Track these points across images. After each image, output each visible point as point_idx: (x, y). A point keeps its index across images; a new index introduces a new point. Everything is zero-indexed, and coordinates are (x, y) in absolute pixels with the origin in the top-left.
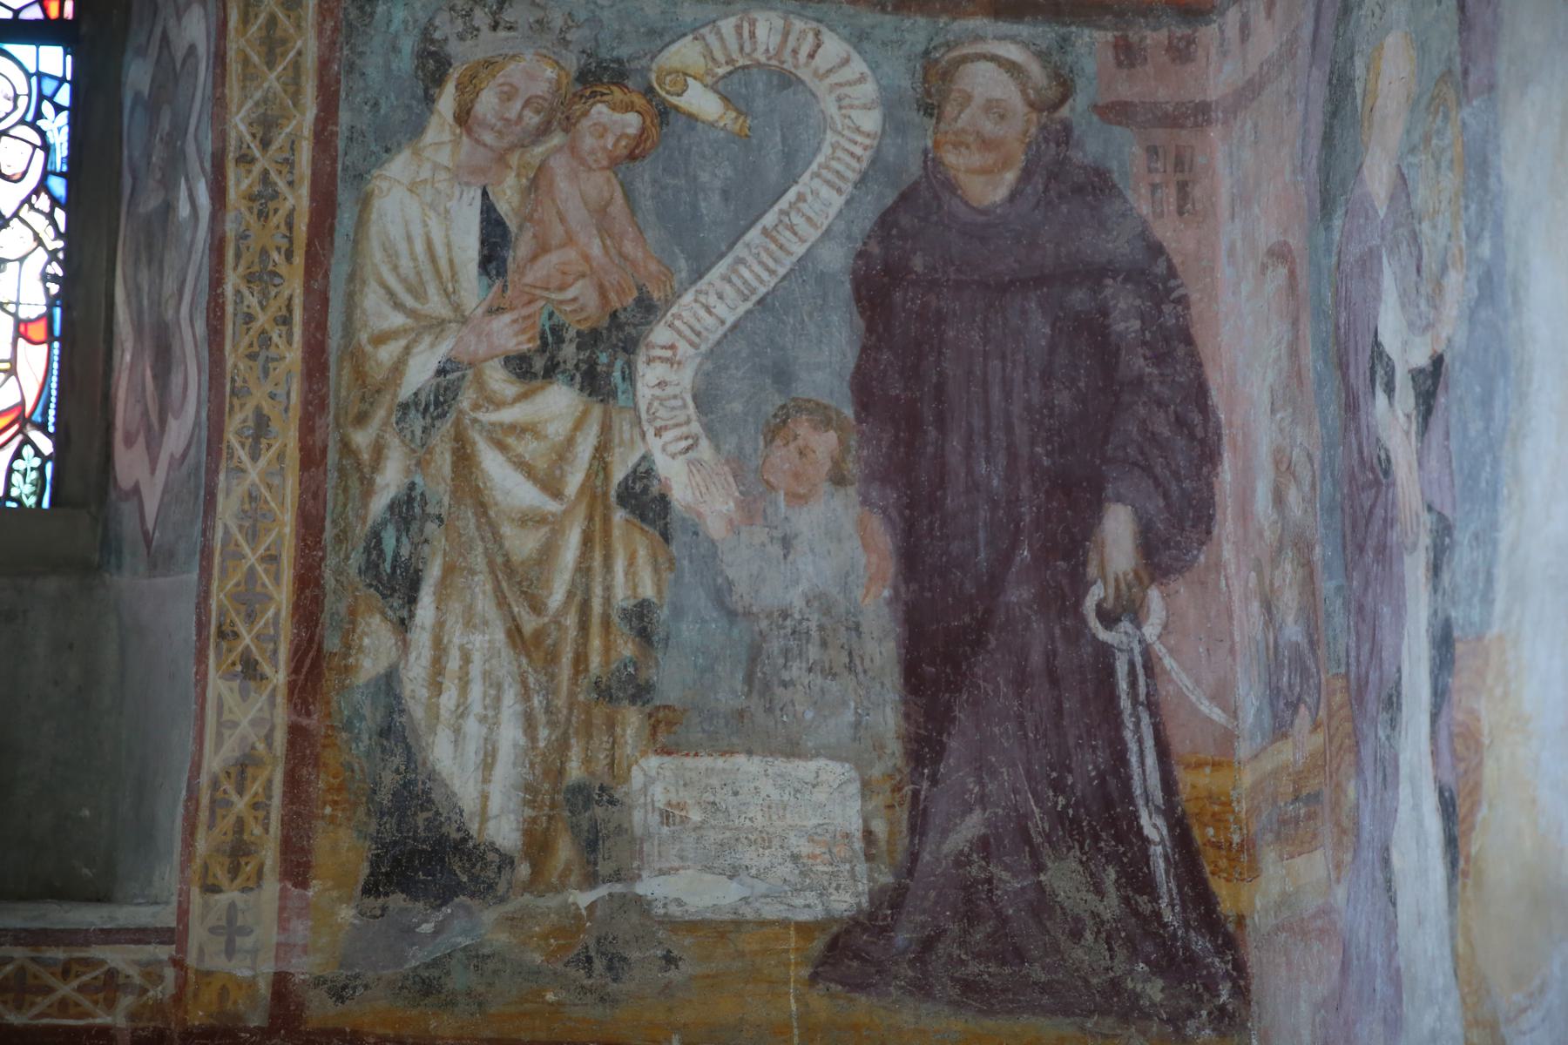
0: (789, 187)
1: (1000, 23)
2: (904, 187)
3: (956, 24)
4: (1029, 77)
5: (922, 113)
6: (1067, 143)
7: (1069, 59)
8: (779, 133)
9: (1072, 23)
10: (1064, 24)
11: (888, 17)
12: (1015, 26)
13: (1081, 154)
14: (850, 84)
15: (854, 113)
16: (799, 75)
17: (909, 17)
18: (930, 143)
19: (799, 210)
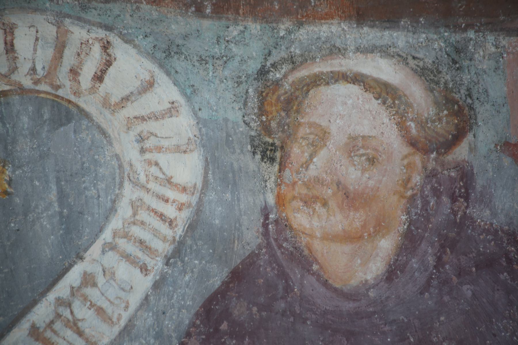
0: (71, 266)
1: (366, 29)
2: (236, 261)
3: (302, 31)
4: (409, 105)
5: (258, 157)
6: (467, 198)
7: (466, 78)
8: (54, 187)
9: (469, 26)
10: (457, 28)
11: (206, 23)
12: (387, 33)
13: (487, 212)
14: (155, 117)
15: (162, 159)
16: (83, 105)
17: (236, 22)
18: (271, 200)
19: (85, 298)
